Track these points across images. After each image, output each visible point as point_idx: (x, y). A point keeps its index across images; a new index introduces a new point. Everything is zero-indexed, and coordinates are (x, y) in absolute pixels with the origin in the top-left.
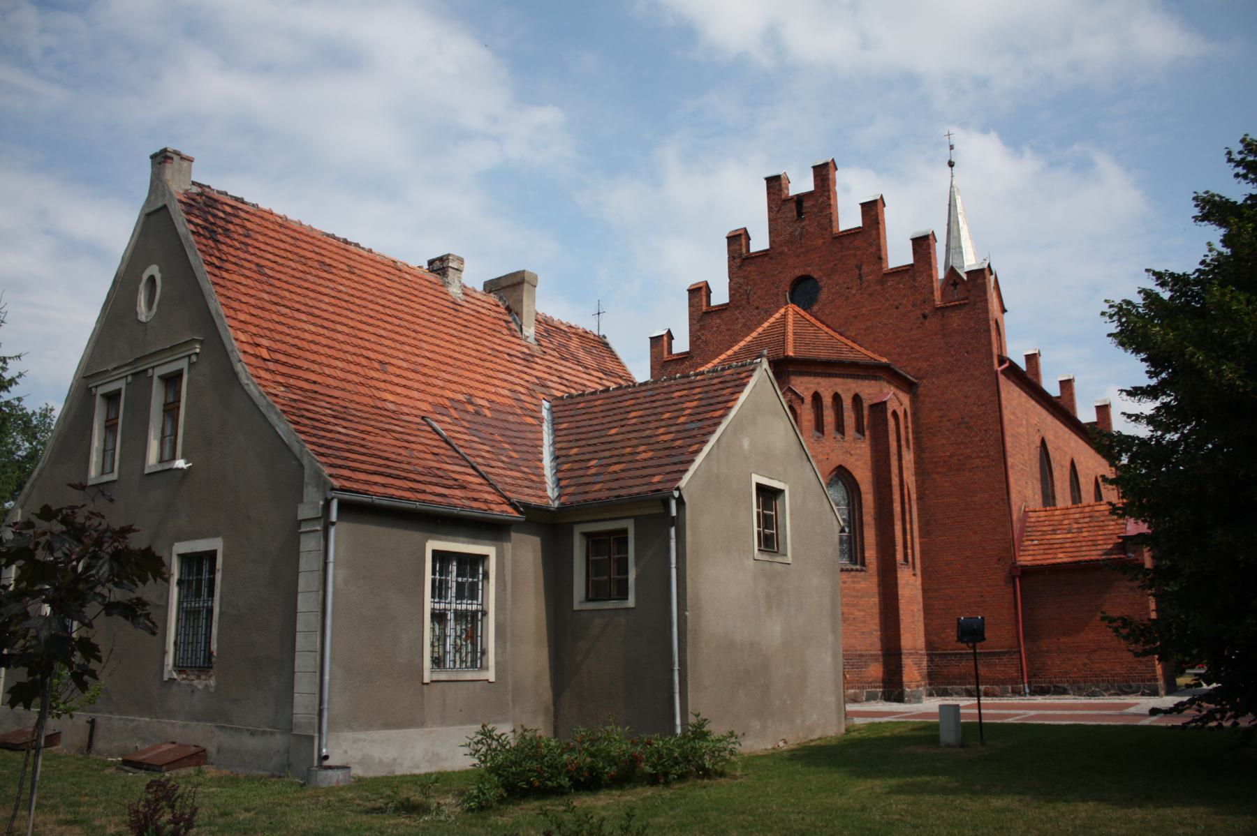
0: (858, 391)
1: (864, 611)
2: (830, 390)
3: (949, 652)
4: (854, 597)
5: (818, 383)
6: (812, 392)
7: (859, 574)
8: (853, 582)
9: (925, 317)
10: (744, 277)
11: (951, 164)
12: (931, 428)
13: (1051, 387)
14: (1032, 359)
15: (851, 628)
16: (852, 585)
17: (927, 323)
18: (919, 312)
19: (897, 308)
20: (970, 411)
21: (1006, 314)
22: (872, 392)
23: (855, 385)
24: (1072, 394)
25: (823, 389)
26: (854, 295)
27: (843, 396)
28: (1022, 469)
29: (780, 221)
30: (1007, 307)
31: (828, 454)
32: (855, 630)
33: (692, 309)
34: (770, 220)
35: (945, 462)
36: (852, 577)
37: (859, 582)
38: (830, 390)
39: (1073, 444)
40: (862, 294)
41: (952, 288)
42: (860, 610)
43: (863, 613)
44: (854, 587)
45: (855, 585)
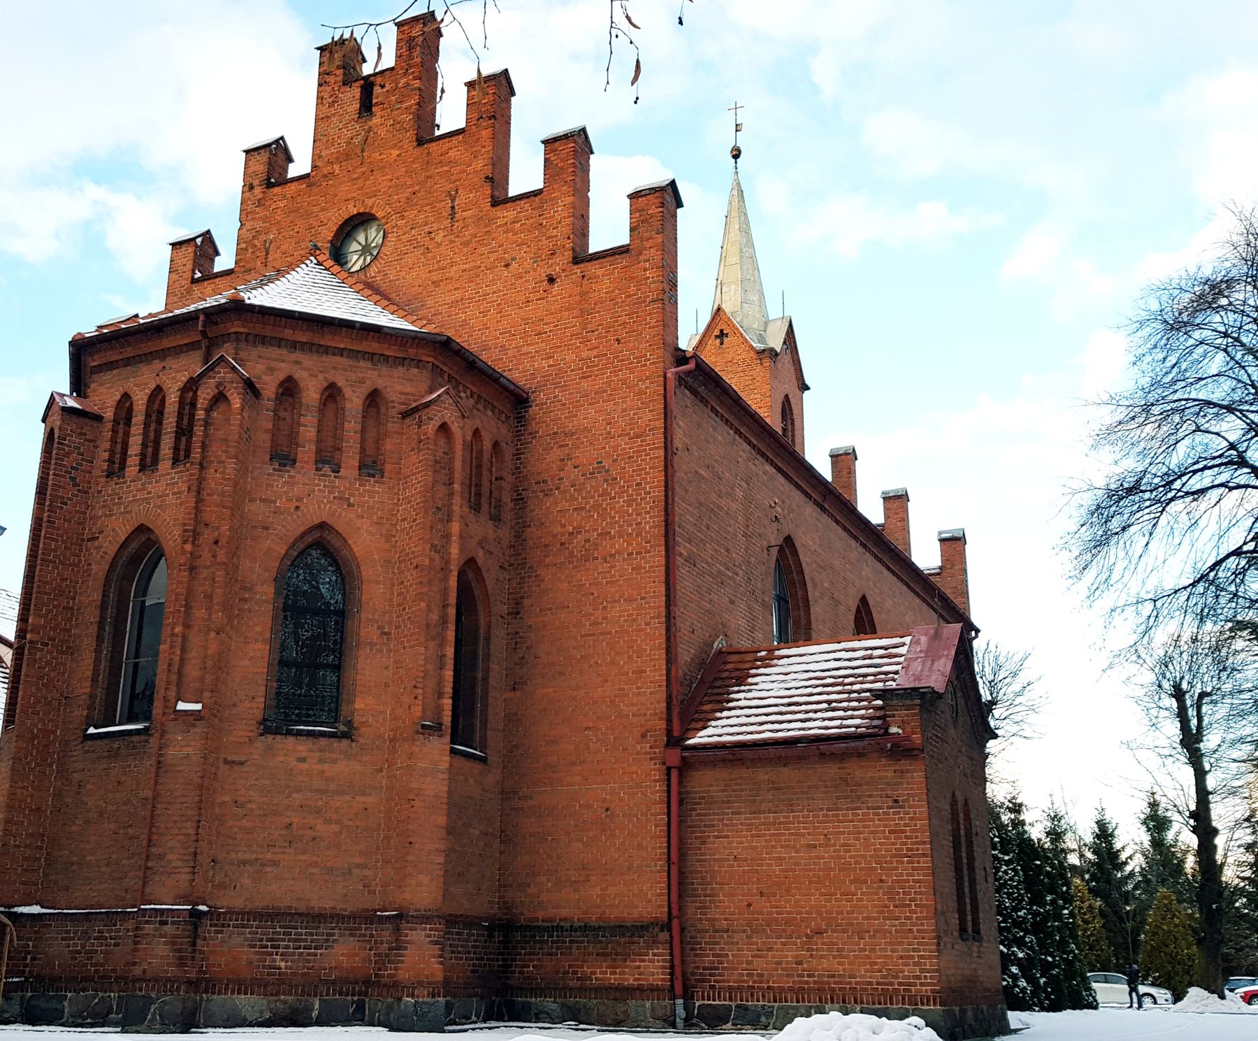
0: (380, 384)
1: (338, 822)
2: (321, 377)
3: (540, 923)
4: (318, 791)
5: (296, 362)
6: (281, 376)
7: (335, 743)
8: (321, 761)
9: (551, 280)
10: (264, 220)
11: (736, 154)
12: (545, 482)
13: (872, 509)
14: (844, 460)
15: (305, 857)
16: (319, 766)
17: (556, 288)
18: (543, 272)
19: (507, 266)
20: (615, 448)
21: (806, 392)
22: (409, 390)
23: (376, 373)
24: (905, 520)
25: (305, 374)
26: (439, 245)
27: (347, 391)
28: (720, 572)
29: (335, 119)
30: (808, 381)
31: (300, 499)
32: (315, 865)
33: (175, 276)
34: (318, 120)
35: (562, 544)
36: (320, 750)
37: (335, 761)
38: (321, 377)
39: (867, 572)
40: (452, 242)
41: (718, 341)
42: (328, 822)
43: (336, 828)
44: (323, 772)
45: (326, 767)
